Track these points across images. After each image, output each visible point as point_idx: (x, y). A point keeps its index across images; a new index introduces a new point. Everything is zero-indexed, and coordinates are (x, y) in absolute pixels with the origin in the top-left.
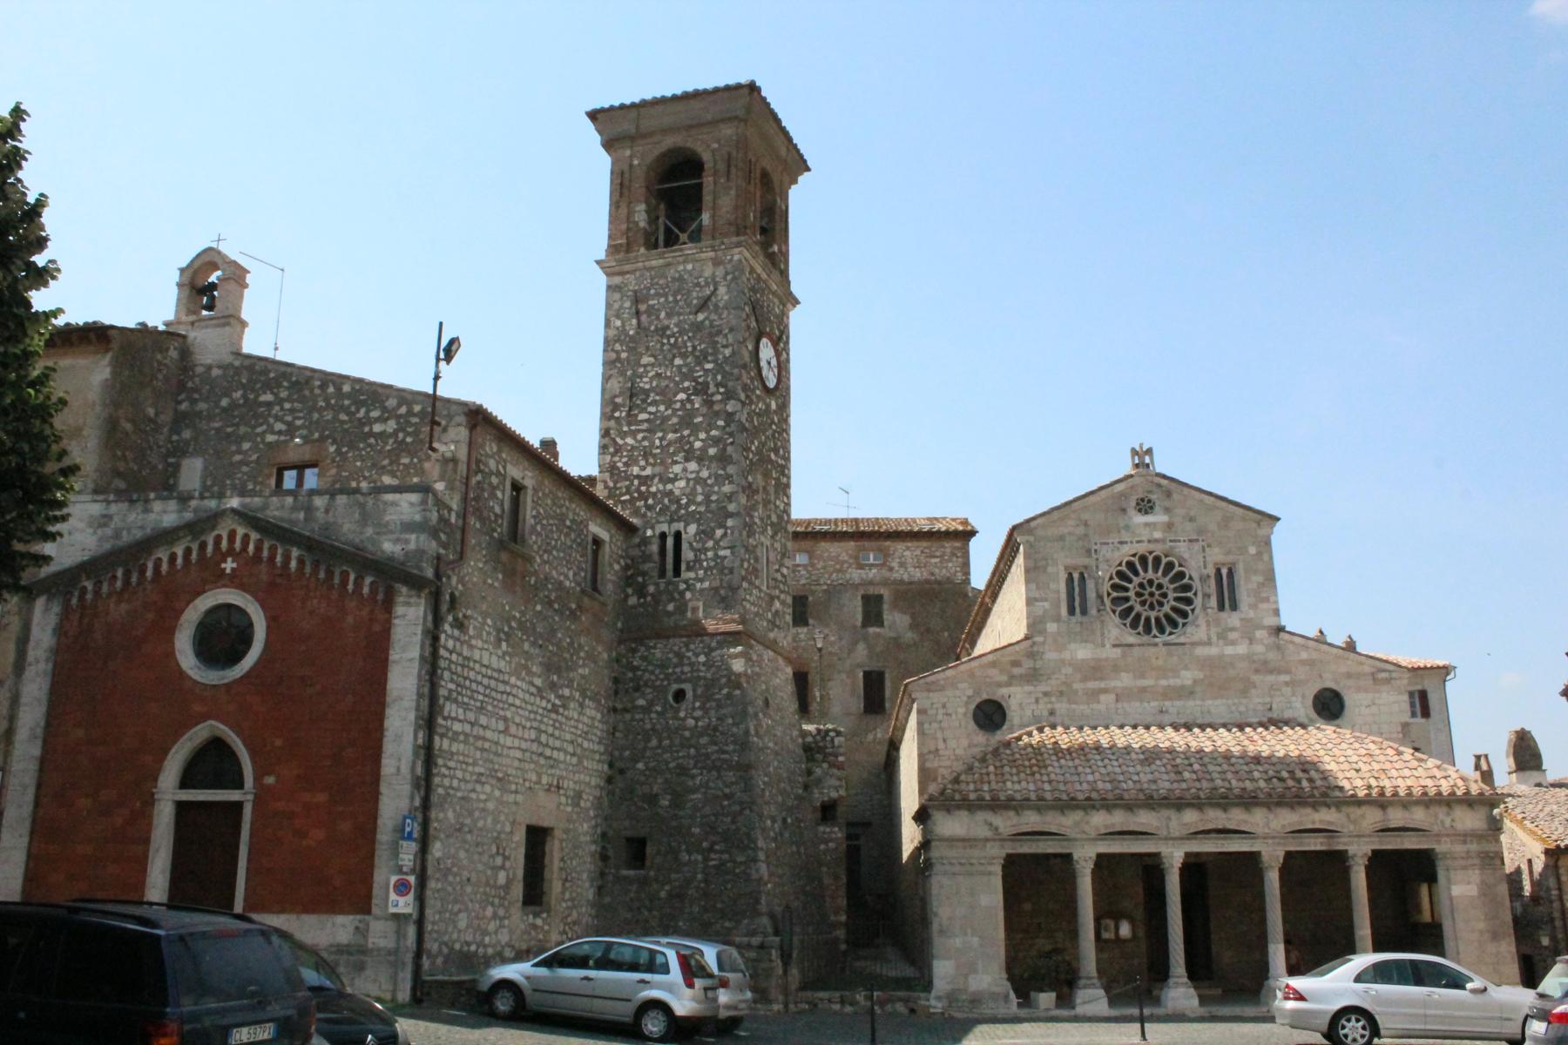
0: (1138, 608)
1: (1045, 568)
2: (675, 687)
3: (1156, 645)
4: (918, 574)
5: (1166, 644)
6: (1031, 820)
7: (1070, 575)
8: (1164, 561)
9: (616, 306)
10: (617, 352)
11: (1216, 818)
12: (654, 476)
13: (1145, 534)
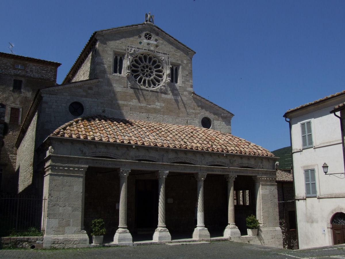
4: (37, 76)
7: (116, 57)
8: (153, 59)
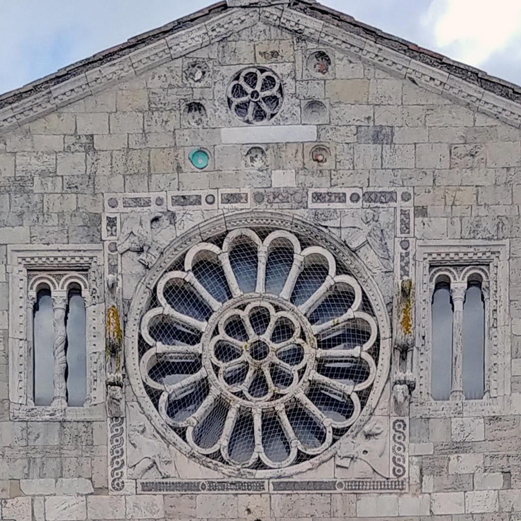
0: (219, 387)
3: (259, 486)
5: (284, 485)
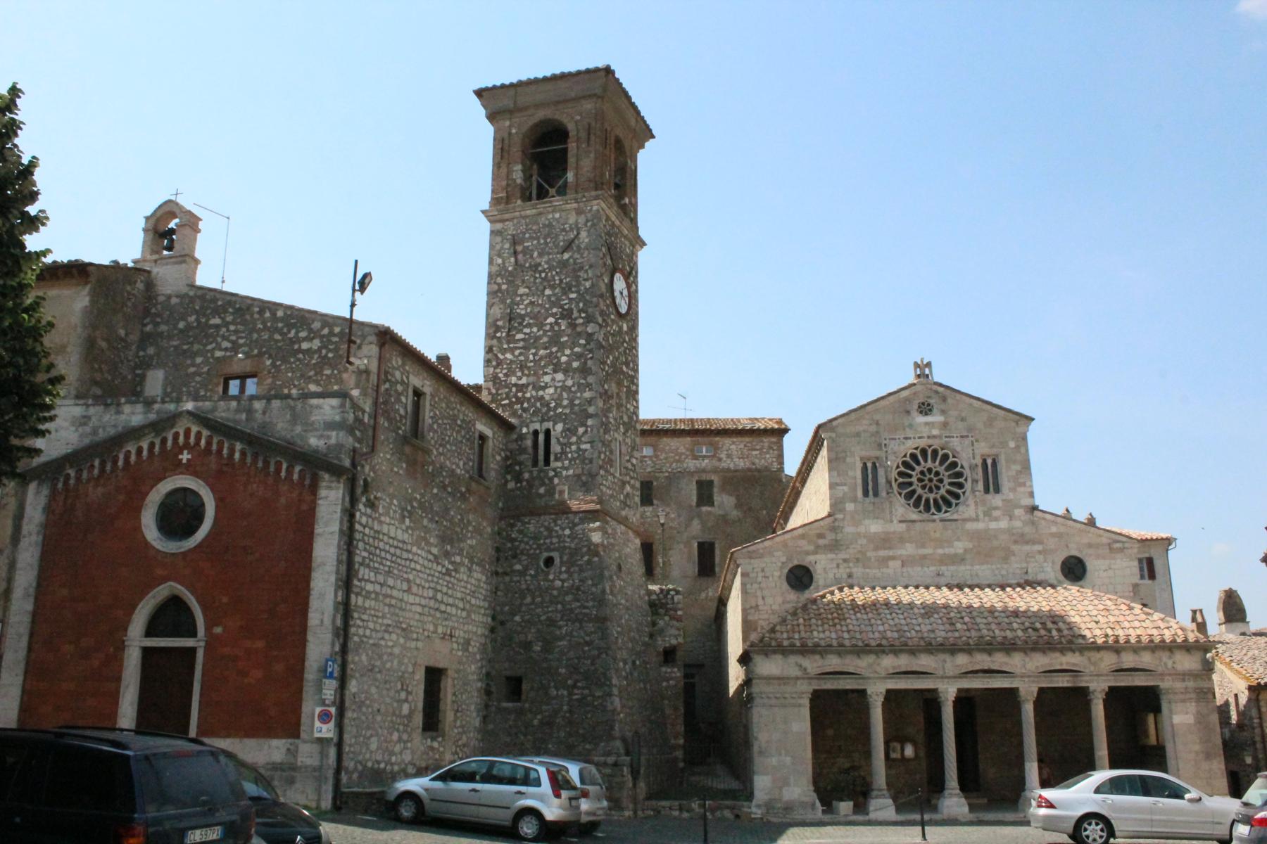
1: (844, 459)
2: (545, 555)
3: (934, 521)
4: (741, 464)
5: (942, 520)
6: (833, 663)
7: (865, 464)
8: (941, 453)
9: (498, 247)
10: (499, 285)
11: (983, 661)
12: (528, 384)
13: (925, 431)
